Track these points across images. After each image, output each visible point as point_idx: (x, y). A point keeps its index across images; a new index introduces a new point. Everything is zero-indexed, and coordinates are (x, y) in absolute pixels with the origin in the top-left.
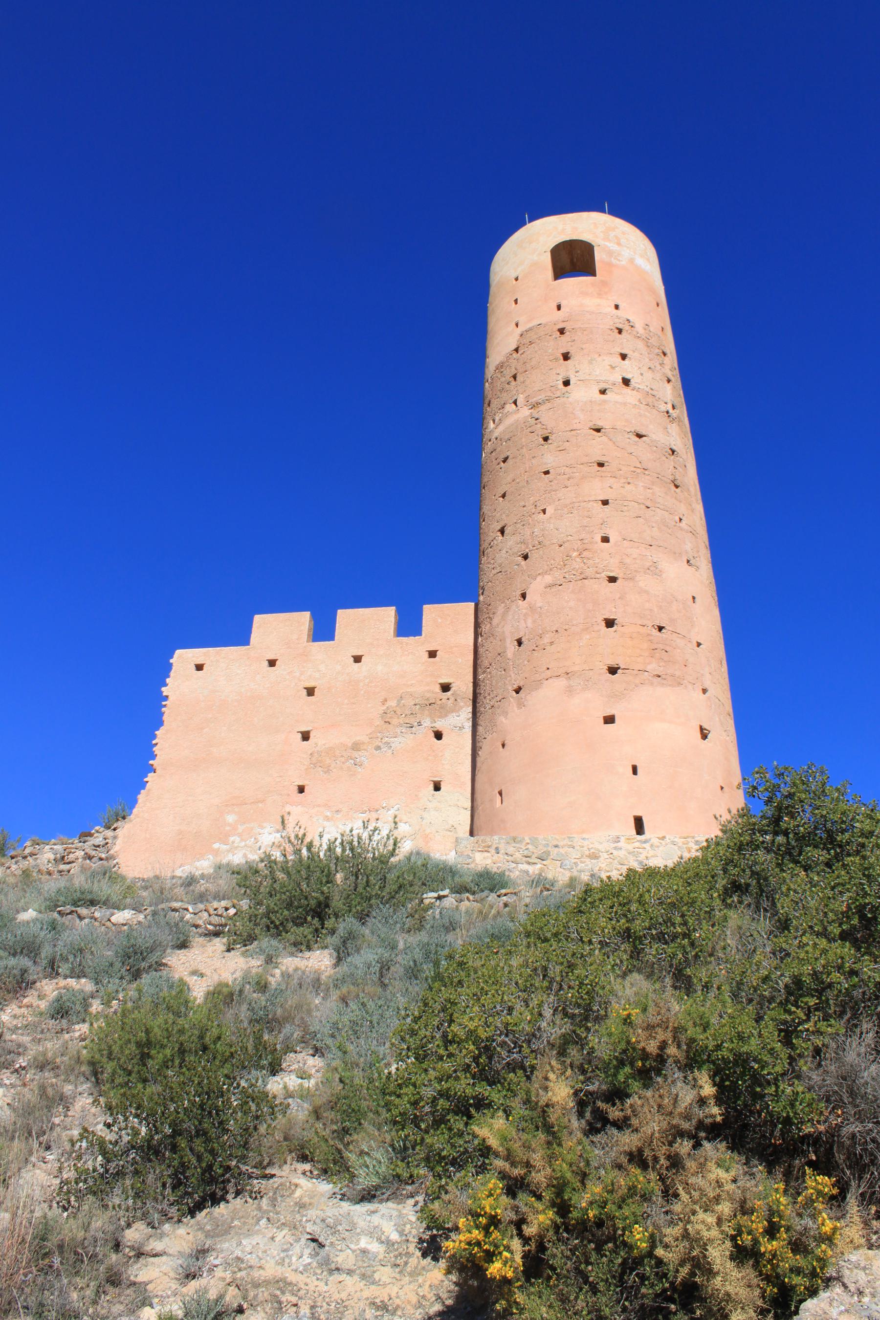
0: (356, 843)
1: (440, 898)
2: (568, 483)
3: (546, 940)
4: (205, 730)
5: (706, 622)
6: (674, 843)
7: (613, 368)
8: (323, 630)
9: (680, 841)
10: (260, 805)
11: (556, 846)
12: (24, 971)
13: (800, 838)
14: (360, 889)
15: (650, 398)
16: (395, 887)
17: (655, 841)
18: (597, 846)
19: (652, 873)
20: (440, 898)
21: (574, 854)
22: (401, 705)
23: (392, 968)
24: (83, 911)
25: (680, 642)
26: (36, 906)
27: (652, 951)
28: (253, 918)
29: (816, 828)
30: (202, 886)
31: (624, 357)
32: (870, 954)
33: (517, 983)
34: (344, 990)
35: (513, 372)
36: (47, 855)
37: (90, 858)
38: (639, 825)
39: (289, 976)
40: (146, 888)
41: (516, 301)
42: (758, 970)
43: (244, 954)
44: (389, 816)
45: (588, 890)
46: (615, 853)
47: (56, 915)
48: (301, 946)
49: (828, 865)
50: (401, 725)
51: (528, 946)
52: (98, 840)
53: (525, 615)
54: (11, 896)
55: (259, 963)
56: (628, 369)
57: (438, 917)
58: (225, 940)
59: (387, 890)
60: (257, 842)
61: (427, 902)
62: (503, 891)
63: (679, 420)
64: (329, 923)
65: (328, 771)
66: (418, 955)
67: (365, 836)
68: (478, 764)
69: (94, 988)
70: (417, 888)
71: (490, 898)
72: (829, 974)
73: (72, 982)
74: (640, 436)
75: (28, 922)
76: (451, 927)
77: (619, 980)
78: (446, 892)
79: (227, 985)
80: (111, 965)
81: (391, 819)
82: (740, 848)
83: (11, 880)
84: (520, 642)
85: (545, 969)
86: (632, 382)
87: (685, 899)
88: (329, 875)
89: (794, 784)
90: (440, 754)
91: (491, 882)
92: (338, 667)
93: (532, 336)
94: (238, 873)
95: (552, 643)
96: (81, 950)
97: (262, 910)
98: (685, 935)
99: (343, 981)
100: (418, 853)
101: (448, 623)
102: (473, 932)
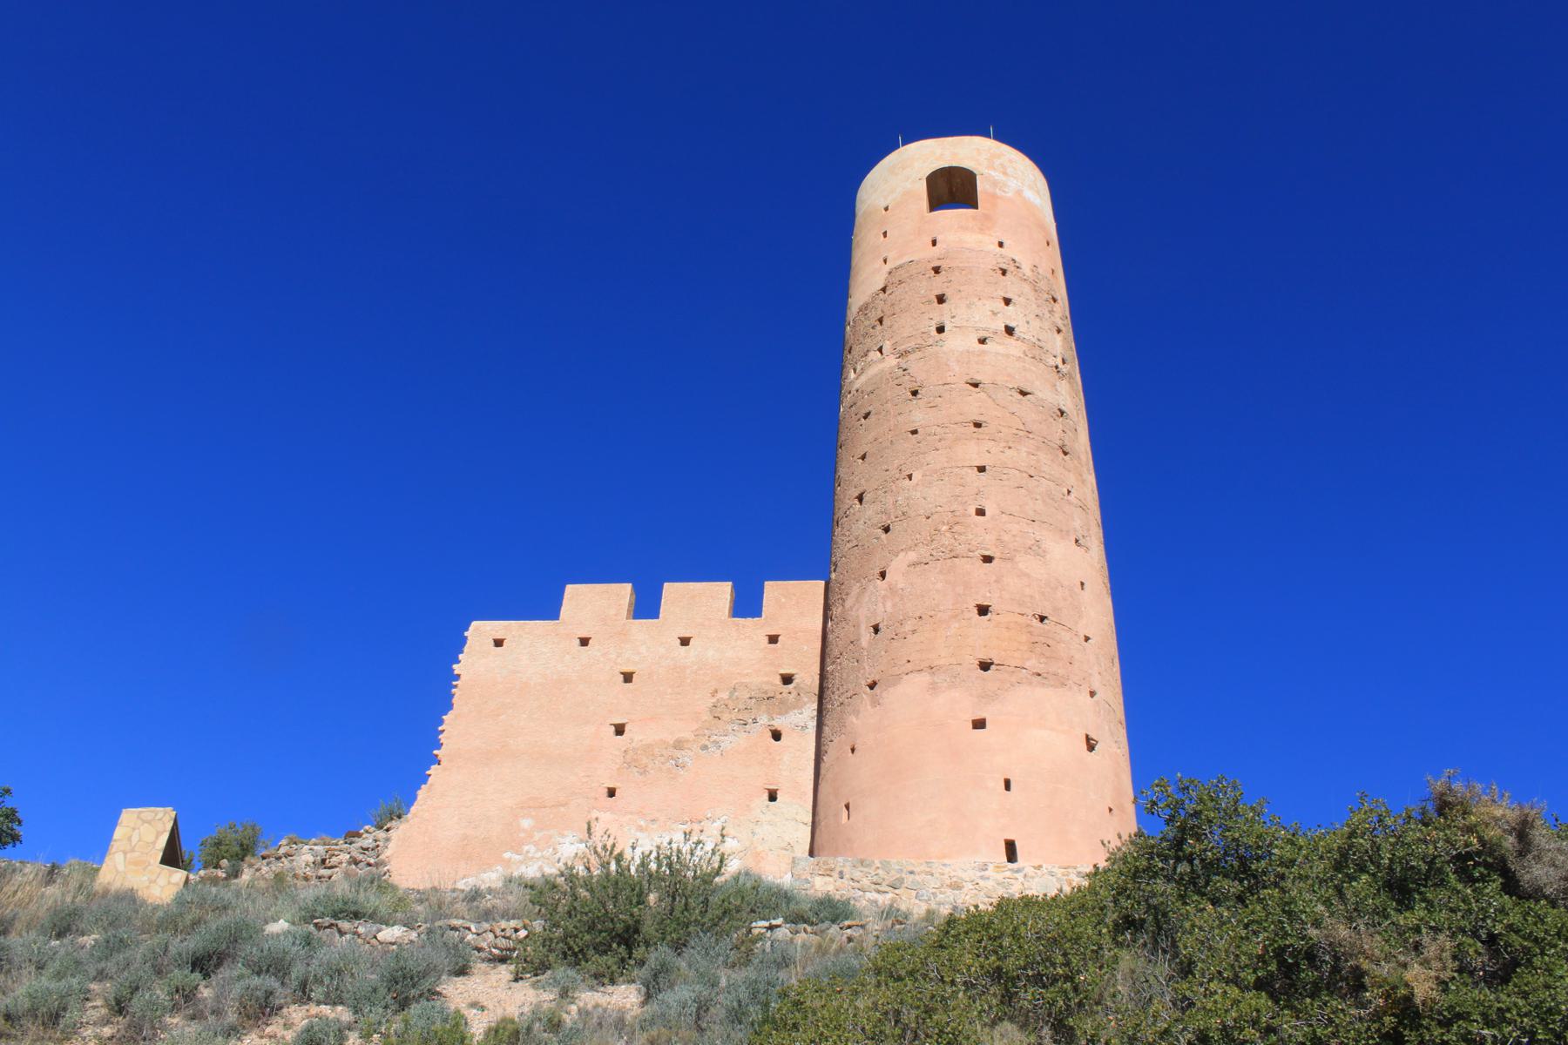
0: (674, 858)
1: (771, 928)
2: (939, 445)
3: (900, 979)
5: (1095, 613)
6: (1052, 874)
7: (994, 314)
8: (646, 606)
9: (1059, 872)
11: (912, 873)
12: (269, 994)
13: (1209, 867)
14: (677, 913)
15: (1037, 351)
16: (719, 912)
17: (1029, 871)
18: (960, 873)
19: (1028, 902)
20: (771, 928)
21: (933, 883)
23: (712, 1010)
24: (345, 925)
25: (1065, 636)
26: (288, 916)
27: (1027, 996)
28: (547, 942)
29: (1226, 854)
30: (487, 902)
31: (1007, 302)
32: (1292, 1008)
33: (863, 1029)
34: (654, 1032)
35: (880, 314)
36: (305, 856)
37: (356, 862)
38: (1011, 851)
39: (588, 1013)
40: (421, 901)
41: (885, 234)
42: (1154, 1024)
43: (535, 986)
44: (713, 830)
45: (951, 921)
46: (982, 883)
47: (311, 928)
48: (604, 978)
49: (1240, 899)
51: (878, 985)
52: (367, 841)
53: (884, 597)
54: (261, 902)
55: (552, 997)
56: (1012, 315)
57: (768, 950)
58: (512, 967)
59: (709, 915)
60: (555, 852)
61: (755, 932)
62: (847, 923)
63: (1070, 377)
64: (639, 953)
65: (644, 772)
66: (744, 994)
67: (686, 849)
68: (823, 771)
69: (352, 1018)
70: (744, 915)
71: (831, 931)
72: (1242, 1029)
73: (325, 1009)
74: (1024, 393)
75: (278, 935)
76: (784, 962)
77: (987, 1030)
78: (779, 921)
79: (512, 1021)
80: (375, 990)
81: (717, 833)
82: (1136, 875)
83: (262, 884)
84: (876, 629)
85: (898, 1013)
86: (1017, 331)
87: (1069, 934)
88: (640, 895)
89: (1201, 800)
91: (833, 911)
92: (662, 651)
93: (902, 274)
94: (532, 887)
95: (914, 632)
96: (339, 972)
97: (559, 933)
98: (1068, 978)
99: (652, 1022)
100: (747, 874)
101: (793, 603)
102: (809, 969)
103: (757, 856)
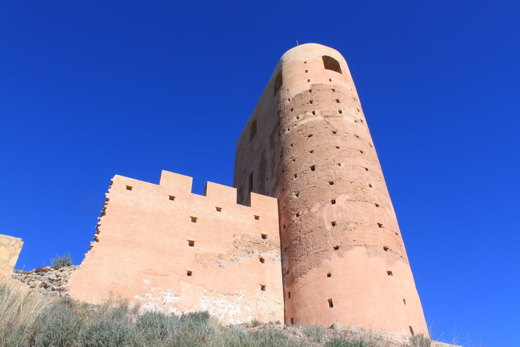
2: (350, 155)
4: (132, 225)
10: (165, 277)
95: (355, 228)
103: (260, 315)
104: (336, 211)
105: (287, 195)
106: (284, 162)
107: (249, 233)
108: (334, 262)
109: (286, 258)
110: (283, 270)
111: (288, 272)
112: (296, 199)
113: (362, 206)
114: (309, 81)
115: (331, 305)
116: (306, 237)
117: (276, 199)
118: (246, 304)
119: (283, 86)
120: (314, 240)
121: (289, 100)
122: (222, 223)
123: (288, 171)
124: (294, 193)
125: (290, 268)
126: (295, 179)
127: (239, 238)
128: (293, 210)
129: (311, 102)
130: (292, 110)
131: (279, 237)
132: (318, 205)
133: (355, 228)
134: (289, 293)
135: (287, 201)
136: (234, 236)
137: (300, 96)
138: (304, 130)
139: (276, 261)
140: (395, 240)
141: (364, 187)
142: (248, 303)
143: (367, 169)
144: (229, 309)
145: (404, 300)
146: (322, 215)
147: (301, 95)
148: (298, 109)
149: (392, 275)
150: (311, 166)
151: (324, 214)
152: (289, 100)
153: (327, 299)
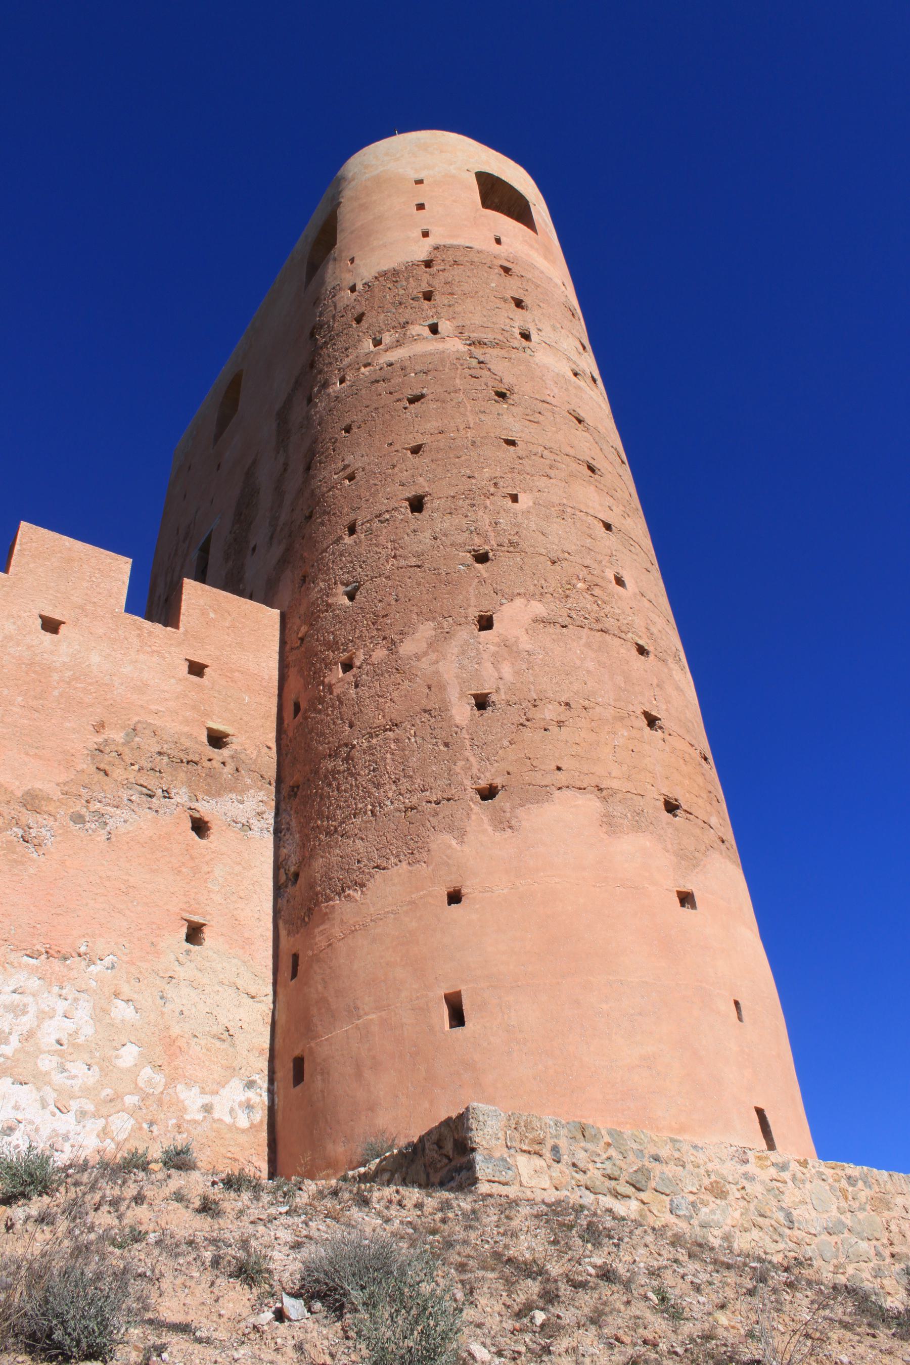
2: (552, 473)
22: (134, 745)
50: (128, 786)
90: (206, 869)
95: (560, 724)
104: (494, 655)
105: (314, 595)
106: (315, 483)
107: (157, 722)
108: (474, 846)
109: (294, 823)
110: (278, 866)
111: (297, 875)
112: (345, 609)
113: (588, 645)
114: (426, 234)
115: (457, 1018)
116: (371, 747)
117: (277, 612)
118: (117, 995)
119: (335, 252)
120: (404, 761)
121: (353, 289)
122: (56, 677)
123: (325, 513)
124: (341, 589)
125: (305, 861)
126: (348, 540)
127: (119, 737)
128: (333, 646)
129: (428, 296)
130: (359, 319)
131: (274, 746)
132: (426, 630)
133: (560, 724)
134: (295, 957)
135: (312, 618)
136: (100, 727)
137: (392, 276)
138: (396, 381)
139: (255, 833)
140: (700, 780)
141: (599, 581)
142: (126, 990)
143: (608, 527)
144: (44, 1016)
145: (737, 1003)
146: (441, 666)
147: (395, 273)
148: (382, 316)
149: (694, 906)
150: (409, 495)
151: (447, 663)
152: (353, 289)
153: (442, 991)
